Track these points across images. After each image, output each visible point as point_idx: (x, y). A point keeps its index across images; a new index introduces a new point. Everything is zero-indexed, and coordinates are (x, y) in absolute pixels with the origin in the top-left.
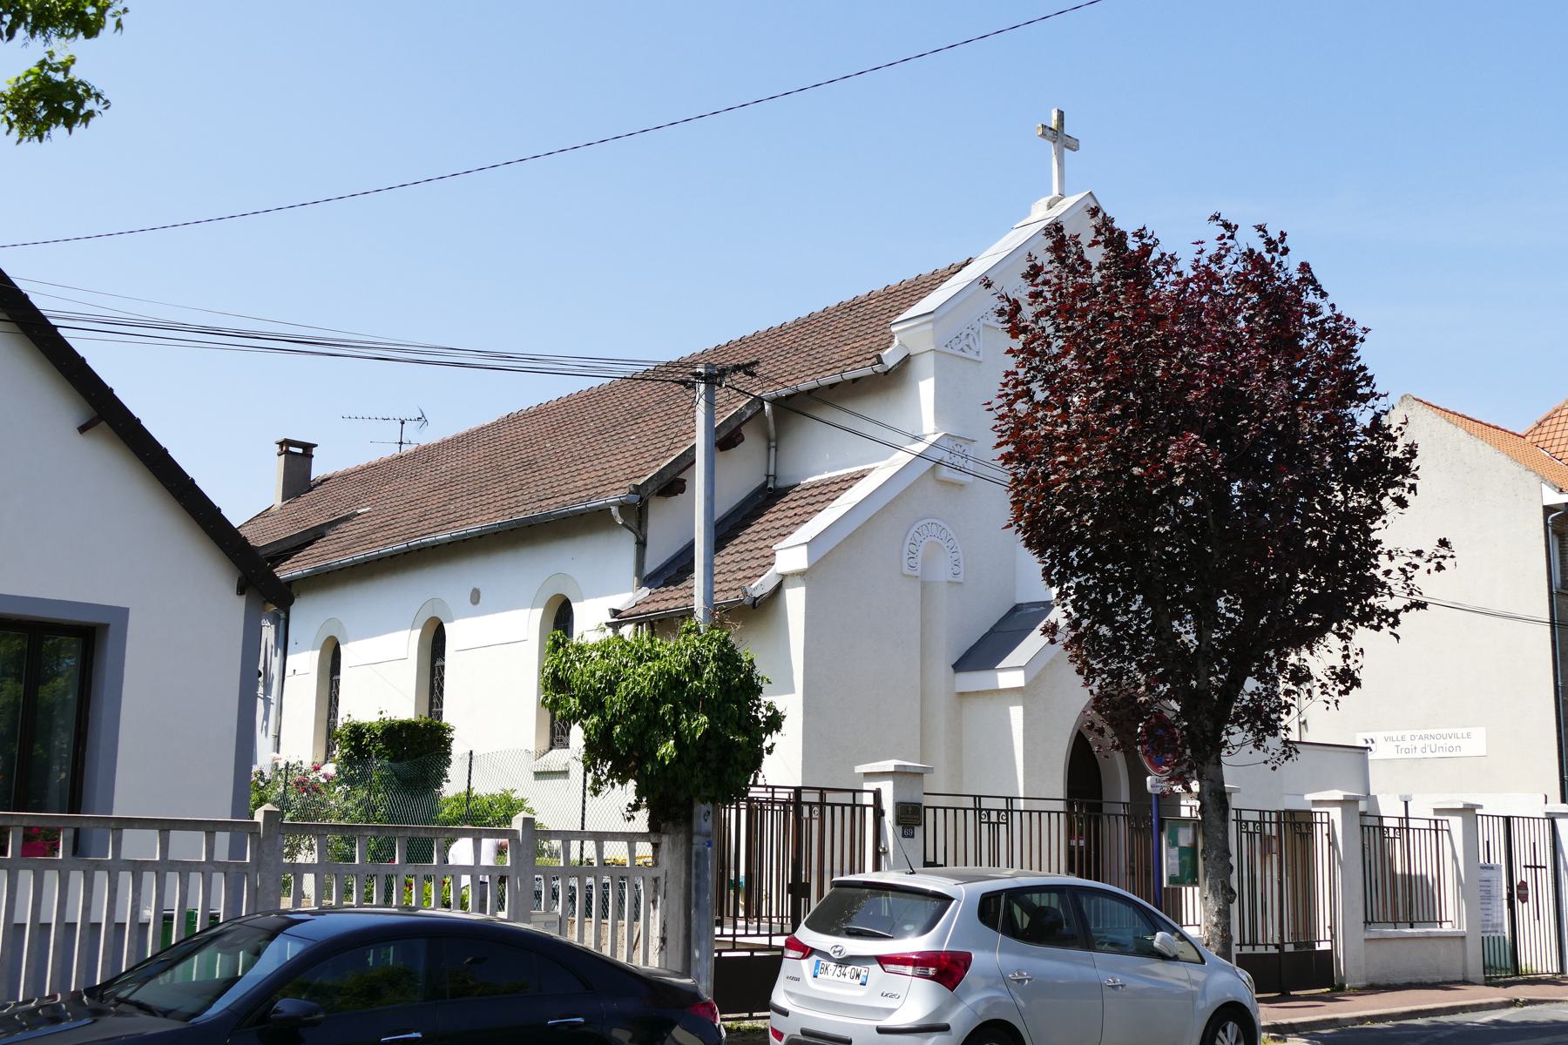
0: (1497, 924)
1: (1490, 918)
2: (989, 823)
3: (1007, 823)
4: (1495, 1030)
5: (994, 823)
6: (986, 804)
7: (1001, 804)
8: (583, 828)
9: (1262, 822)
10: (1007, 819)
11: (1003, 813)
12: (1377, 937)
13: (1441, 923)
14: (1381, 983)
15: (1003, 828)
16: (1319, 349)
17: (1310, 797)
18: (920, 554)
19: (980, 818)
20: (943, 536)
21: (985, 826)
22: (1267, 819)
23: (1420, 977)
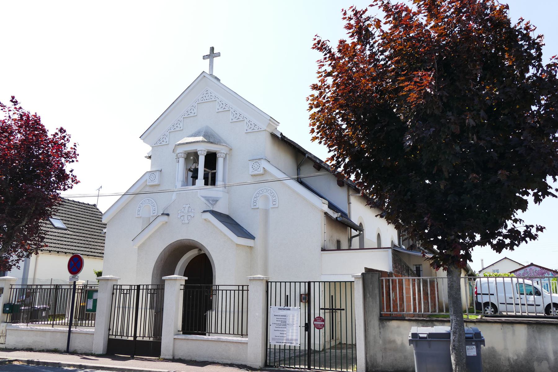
0: (292, 340)
1: (285, 335)
2: (124, 293)
3: (129, 294)
5: (125, 294)
6: (123, 287)
8: (325, 307)
9: (131, 289)
10: (130, 292)
11: (128, 290)
15: (128, 295)
16: (334, 89)
18: (137, 212)
19: (148, 292)
21: (122, 295)
22: (133, 288)
23: (181, 357)
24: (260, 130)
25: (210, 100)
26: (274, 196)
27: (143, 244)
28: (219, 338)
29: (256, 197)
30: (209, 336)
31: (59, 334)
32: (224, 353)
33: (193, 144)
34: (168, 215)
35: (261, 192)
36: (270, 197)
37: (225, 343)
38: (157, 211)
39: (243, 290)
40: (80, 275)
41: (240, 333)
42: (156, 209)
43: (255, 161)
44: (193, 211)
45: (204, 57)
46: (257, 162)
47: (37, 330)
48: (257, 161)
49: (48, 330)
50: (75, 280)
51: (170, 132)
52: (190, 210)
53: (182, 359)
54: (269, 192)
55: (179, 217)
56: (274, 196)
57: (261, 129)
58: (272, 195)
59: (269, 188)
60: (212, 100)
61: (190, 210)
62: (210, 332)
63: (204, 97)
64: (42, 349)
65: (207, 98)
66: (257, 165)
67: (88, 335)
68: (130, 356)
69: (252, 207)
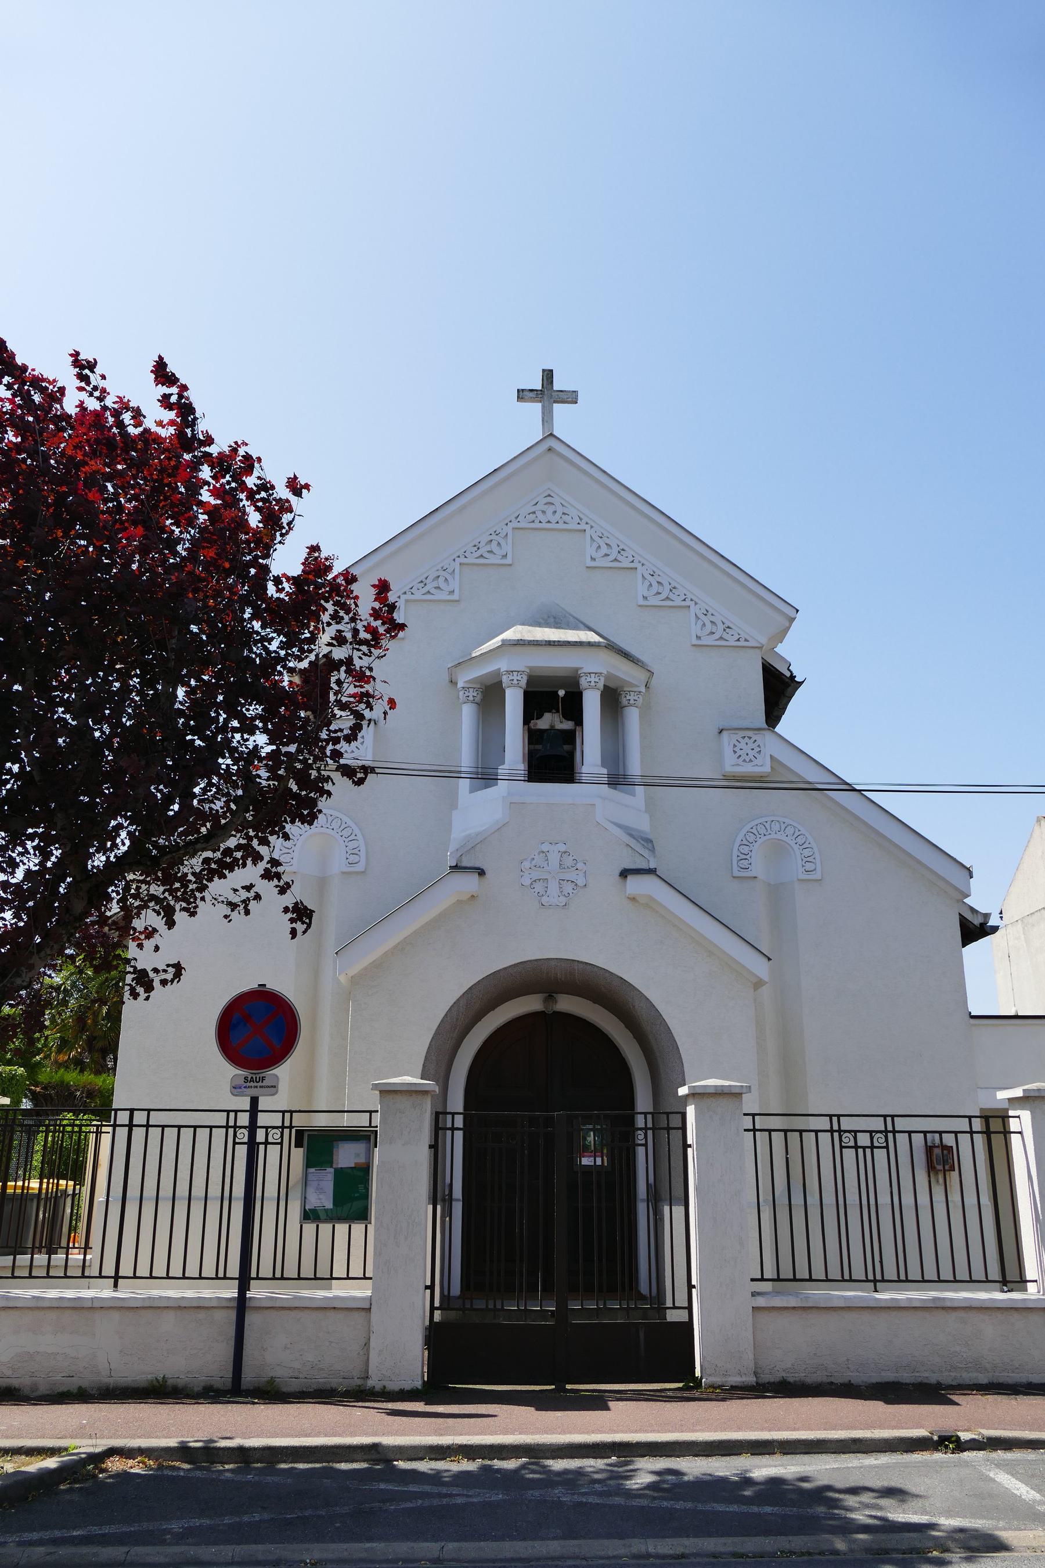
3: (887, 1147)
4: (110, 1483)
6: (846, 1124)
7: (878, 1124)
12: (48, 1305)
13: (117, 1277)
14: (809, 1380)
15: (880, 1155)
17: (1003, 1095)
19: (841, 1140)
20: (335, 825)
23: (784, 1375)
24: (742, 643)
25: (561, 526)
26: (805, 846)
27: (378, 967)
28: (939, 1298)
29: (745, 842)
30: (876, 1291)
31: (171, 1316)
32: (958, 1348)
33: (593, 649)
34: (481, 873)
35: (762, 831)
36: (796, 847)
37: (962, 1314)
38: (367, 859)
39: (131, 1126)
40: (283, 1072)
41: (994, 1273)
42: (363, 848)
43: (742, 733)
44: (580, 866)
45: (522, 395)
46: (750, 738)
47: (41, 1304)
48: (750, 733)
49: (147, 1304)
50: (254, 1092)
51: (407, 601)
52: (568, 861)
53: (791, 1380)
54: (790, 831)
55: (527, 882)
56: (805, 846)
57: (746, 640)
58: (800, 840)
59: (788, 821)
60: (565, 526)
61: (568, 861)
62: (879, 1277)
63: (539, 514)
64: (73, 1385)
65: (549, 516)
66: (751, 745)
67: (331, 1314)
68: (553, 1387)
69: (736, 873)
